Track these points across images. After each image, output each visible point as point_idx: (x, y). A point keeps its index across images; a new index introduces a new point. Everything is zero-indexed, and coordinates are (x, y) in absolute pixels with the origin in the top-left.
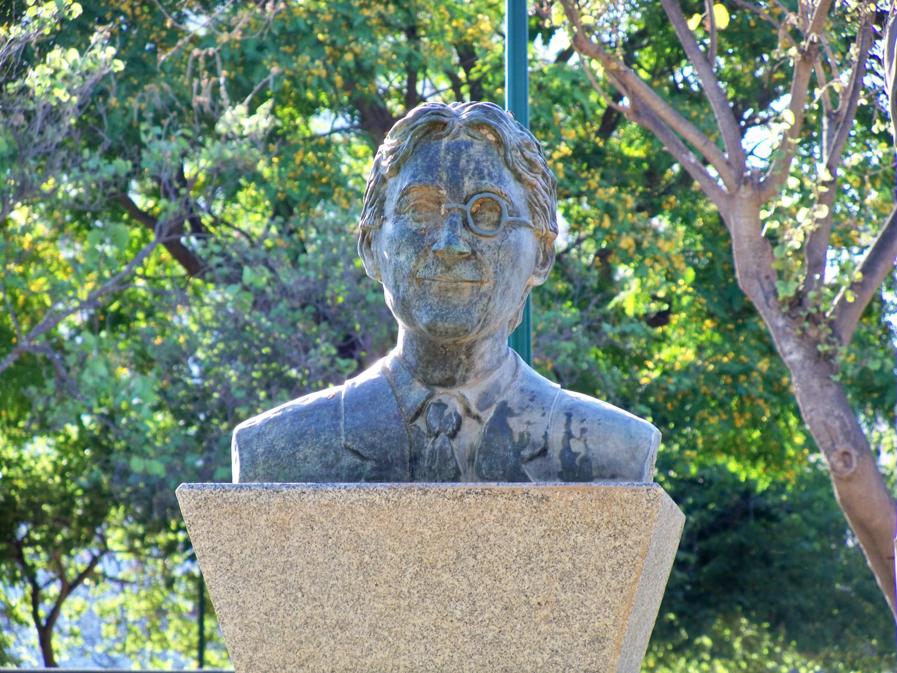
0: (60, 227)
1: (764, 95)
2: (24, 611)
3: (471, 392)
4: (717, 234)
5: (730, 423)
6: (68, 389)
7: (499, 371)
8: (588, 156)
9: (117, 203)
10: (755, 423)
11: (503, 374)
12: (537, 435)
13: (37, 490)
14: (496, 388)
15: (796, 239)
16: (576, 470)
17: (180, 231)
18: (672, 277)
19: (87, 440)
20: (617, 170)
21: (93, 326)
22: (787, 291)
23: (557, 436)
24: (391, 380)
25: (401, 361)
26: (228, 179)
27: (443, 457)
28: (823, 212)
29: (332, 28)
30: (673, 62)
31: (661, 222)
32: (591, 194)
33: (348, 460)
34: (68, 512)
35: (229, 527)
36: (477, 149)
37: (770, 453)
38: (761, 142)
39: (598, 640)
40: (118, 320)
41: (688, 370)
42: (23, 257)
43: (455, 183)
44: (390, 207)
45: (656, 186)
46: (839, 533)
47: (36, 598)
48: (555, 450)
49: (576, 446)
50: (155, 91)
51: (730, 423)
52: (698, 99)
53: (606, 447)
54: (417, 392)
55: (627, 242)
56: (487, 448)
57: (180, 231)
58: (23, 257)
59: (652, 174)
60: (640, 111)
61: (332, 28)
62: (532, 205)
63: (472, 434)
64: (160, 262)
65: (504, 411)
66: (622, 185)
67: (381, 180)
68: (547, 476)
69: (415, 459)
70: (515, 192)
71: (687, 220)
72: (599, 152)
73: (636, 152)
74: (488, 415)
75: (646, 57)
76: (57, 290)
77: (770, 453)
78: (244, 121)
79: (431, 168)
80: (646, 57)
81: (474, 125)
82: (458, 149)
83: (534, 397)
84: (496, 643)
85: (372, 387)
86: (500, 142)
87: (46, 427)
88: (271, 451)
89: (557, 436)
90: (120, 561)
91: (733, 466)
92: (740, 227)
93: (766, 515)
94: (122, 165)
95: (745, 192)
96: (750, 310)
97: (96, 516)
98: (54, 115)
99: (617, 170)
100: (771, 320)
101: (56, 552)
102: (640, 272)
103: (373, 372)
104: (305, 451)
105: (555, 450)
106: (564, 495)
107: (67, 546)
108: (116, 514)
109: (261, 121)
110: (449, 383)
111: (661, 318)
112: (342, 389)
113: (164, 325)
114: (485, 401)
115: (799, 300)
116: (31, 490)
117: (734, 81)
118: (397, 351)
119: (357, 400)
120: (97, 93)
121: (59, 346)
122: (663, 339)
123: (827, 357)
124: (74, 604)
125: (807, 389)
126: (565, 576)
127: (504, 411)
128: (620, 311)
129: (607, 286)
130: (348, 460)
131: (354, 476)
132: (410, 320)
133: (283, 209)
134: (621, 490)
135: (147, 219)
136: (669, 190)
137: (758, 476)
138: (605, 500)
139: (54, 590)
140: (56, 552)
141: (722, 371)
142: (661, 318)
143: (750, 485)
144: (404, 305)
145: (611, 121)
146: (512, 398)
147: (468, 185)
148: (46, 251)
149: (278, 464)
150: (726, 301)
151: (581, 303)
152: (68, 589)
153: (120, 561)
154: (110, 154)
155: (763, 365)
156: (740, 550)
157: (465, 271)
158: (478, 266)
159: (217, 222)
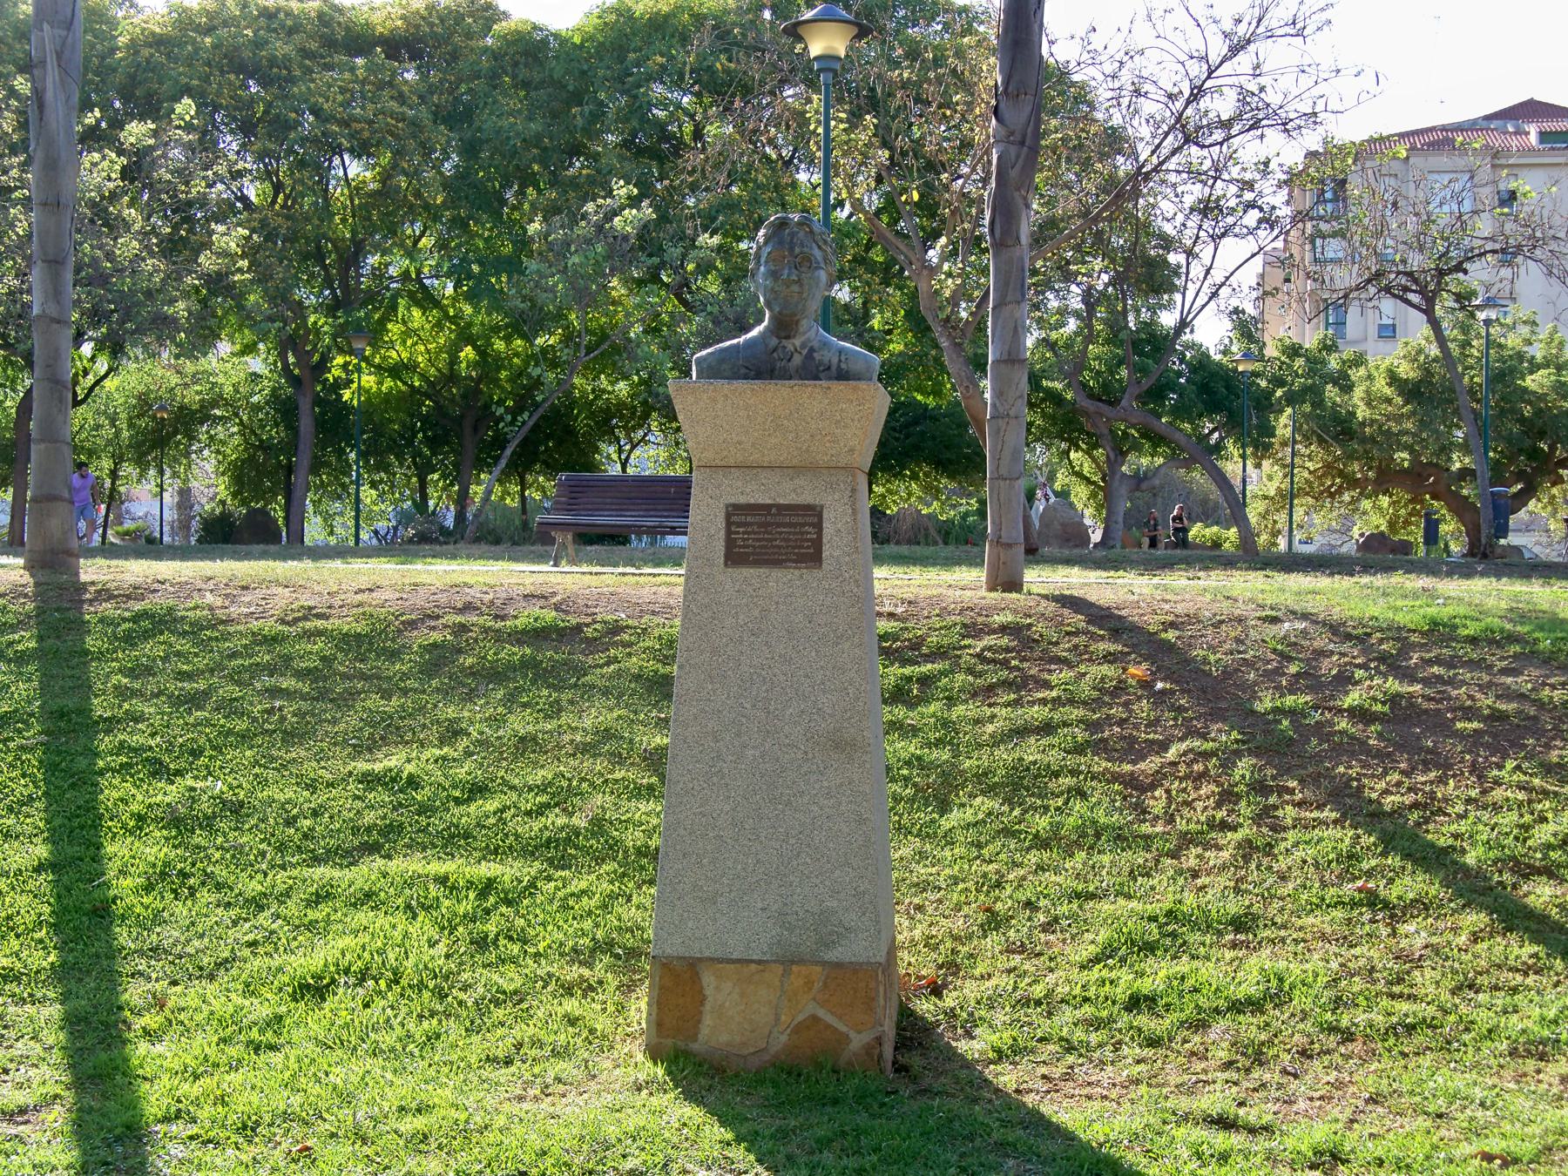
0: (631, 290)
1: (936, 235)
2: (615, 457)
3: (797, 342)
4: (914, 295)
5: (918, 377)
6: (633, 358)
7: (812, 332)
8: (859, 260)
9: (656, 279)
10: (930, 379)
11: (812, 333)
12: (826, 360)
13: (621, 405)
14: (809, 340)
15: (947, 293)
16: (843, 376)
17: (681, 289)
18: (895, 314)
19: (642, 382)
20: (871, 267)
21: (645, 332)
22: (942, 316)
23: (835, 361)
24: (762, 335)
25: (767, 328)
26: (704, 268)
27: (785, 369)
28: (959, 282)
29: (749, 203)
30: (896, 222)
31: (890, 290)
32: (860, 277)
33: (743, 371)
34: (634, 413)
35: (691, 399)
36: (801, 234)
37: (937, 392)
38: (933, 255)
39: (852, 450)
40: (657, 330)
41: (901, 353)
42: (614, 303)
43: (791, 249)
44: (763, 260)
45: (888, 274)
46: (966, 425)
47: (620, 451)
48: (834, 368)
49: (843, 366)
50: (671, 228)
51: (918, 377)
52: (907, 237)
53: (856, 366)
54: (774, 342)
55: (875, 298)
56: (804, 366)
57: (681, 289)
58: (614, 303)
59: (886, 268)
60: (881, 236)
61: (749, 203)
62: (825, 259)
63: (797, 359)
64: (672, 305)
65: (812, 350)
66: (873, 273)
67: (759, 248)
68: (830, 379)
69: (772, 371)
70: (818, 254)
71: (901, 289)
72: (864, 259)
73: (880, 259)
74: (805, 352)
75: (885, 218)
76: (628, 315)
77: (937, 392)
78: (705, 239)
79: (781, 243)
80: (885, 218)
81: (800, 224)
82: (793, 235)
83: (825, 344)
84: (807, 451)
85: (754, 339)
86: (812, 232)
87: (626, 377)
88: (710, 367)
89: (835, 361)
90: (656, 436)
91: (919, 397)
92: (923, 287)
93: (934, 419)
94: (656, 260)
95: (925, 272)
96: (929, 328)
97: (646, 416)
98: (626, 238)
99: (871, 267)
100: (937, 330)
101: (629, 431)
102: (881, 312)
103: (755, 332)
104: (724, 366)
105: (834, 368)
106: (838, 387)
107: (634, 429)
108: (654, 415)
109: (716, 240)
110: (787, 337)
111: (890, 332)
112: (741, 340)
113: (676, 333)
114: (803, 345)
115: (948, 320)
116: (618, 405)
117: (923, 229)
118: (765, 323)
119: (748, 343)
120: (645, 228)
121: (629, 340)
122: (891, 341)
123: (960, 345)
124: (637, 452)
125: (951, 359)
126: (838, 422)
127: (812, 350)
128: (872, 328)
129: (867, 317)
130: (743, 371)
131: (746, 377)
132: (771, 310)
133: (727, 281)
134: (862, 385)
135: (667, 285)
136: (894, 276)
137: (931, 401)
138: (855, 389)
139: (628, 447)
140: (629, 431)
141: (915, 355)
142: (890, 332)
143: (926, 405)
144: (768, 304)
145: (868, 248)
146: (816, 344)
147: (797, 250)
148: (625, 300)
149: (712, 371)
150: (917, 323)
151: (855, 325)
152: (634, 447)
153: (656, 436)
154: (650, 255)
155: (933, 352)
156: (923, 433)
157: (795, 288)
158: (801, 286)
159: (699, 288)
